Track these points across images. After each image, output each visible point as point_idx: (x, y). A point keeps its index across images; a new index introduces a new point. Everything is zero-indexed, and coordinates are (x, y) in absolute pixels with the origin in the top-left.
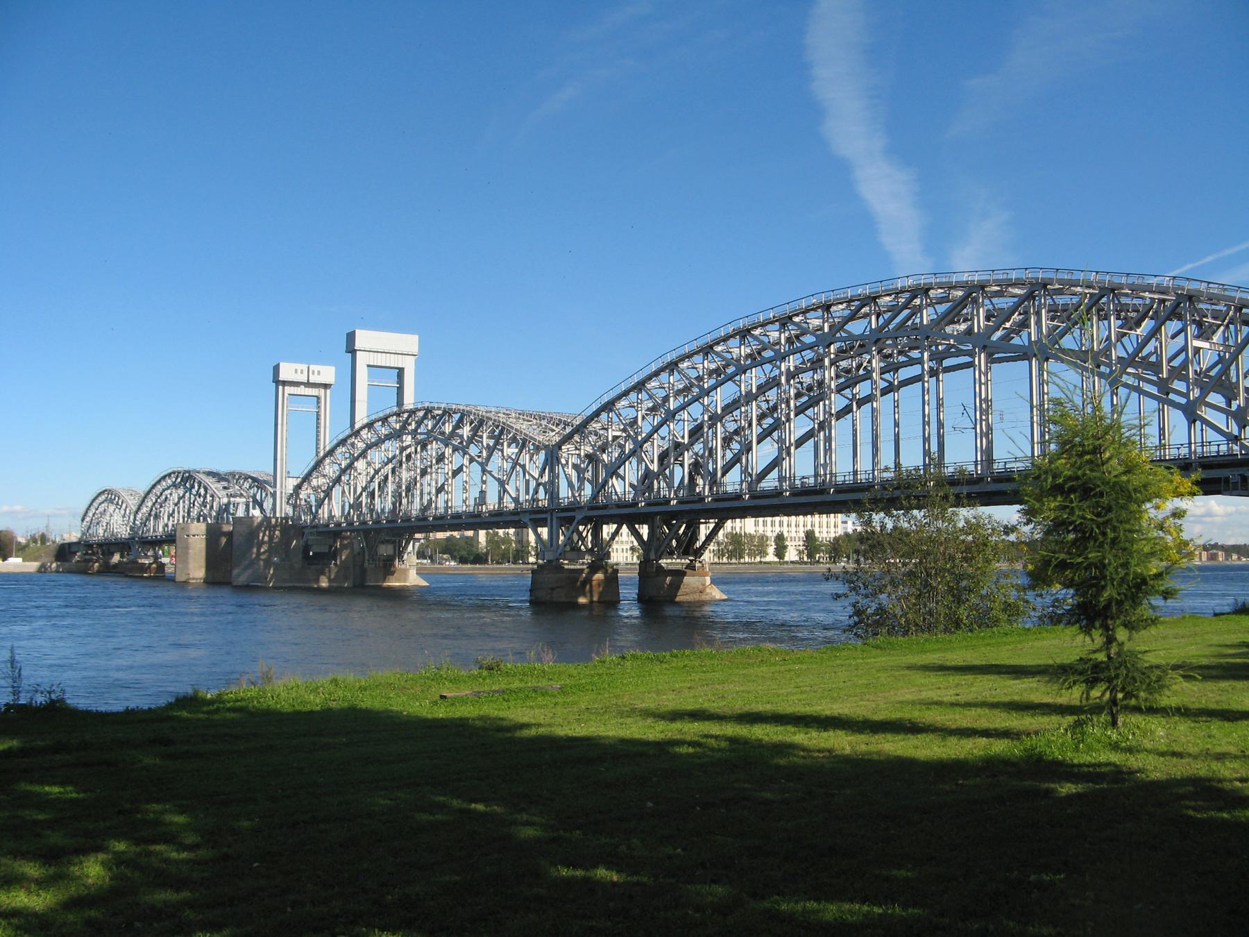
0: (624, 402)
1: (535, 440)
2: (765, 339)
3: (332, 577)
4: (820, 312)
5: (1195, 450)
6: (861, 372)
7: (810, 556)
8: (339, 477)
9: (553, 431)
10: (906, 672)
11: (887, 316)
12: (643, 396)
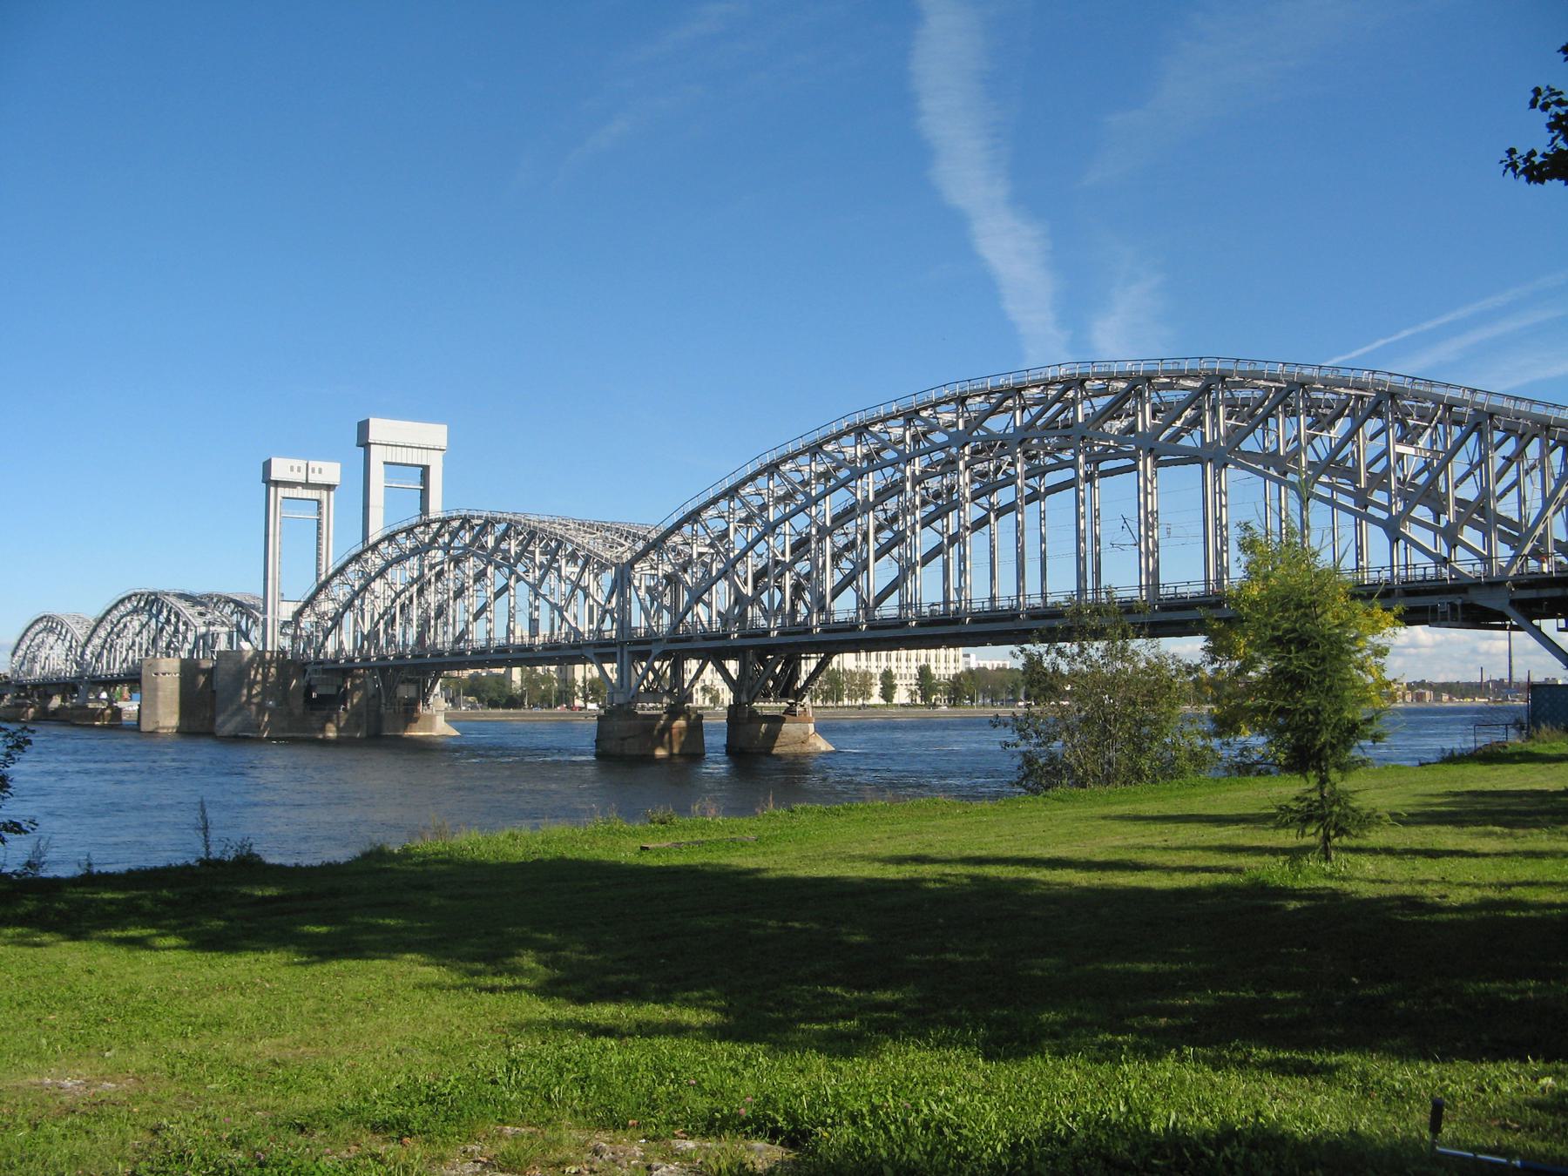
0: (712, 512)
1: (602, 557)
2: (886, 437)
3: (342, 724)
4: (953, 405)
5: (1398, 574)
6: (1000, 477)
7: (925, 697)
9: (622, 545)
10: (1103, 822)
11: (1035, 410)
12: (736, 504)
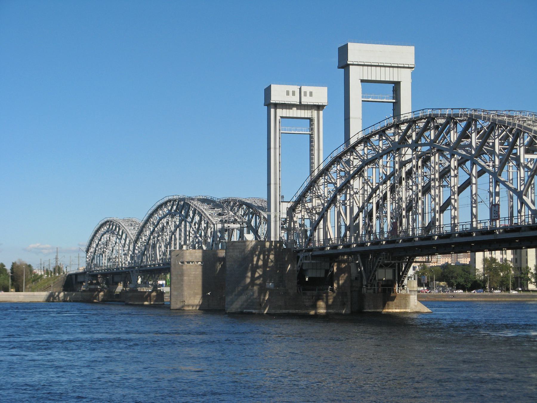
3: (330, 301)
8: (335, 197)
